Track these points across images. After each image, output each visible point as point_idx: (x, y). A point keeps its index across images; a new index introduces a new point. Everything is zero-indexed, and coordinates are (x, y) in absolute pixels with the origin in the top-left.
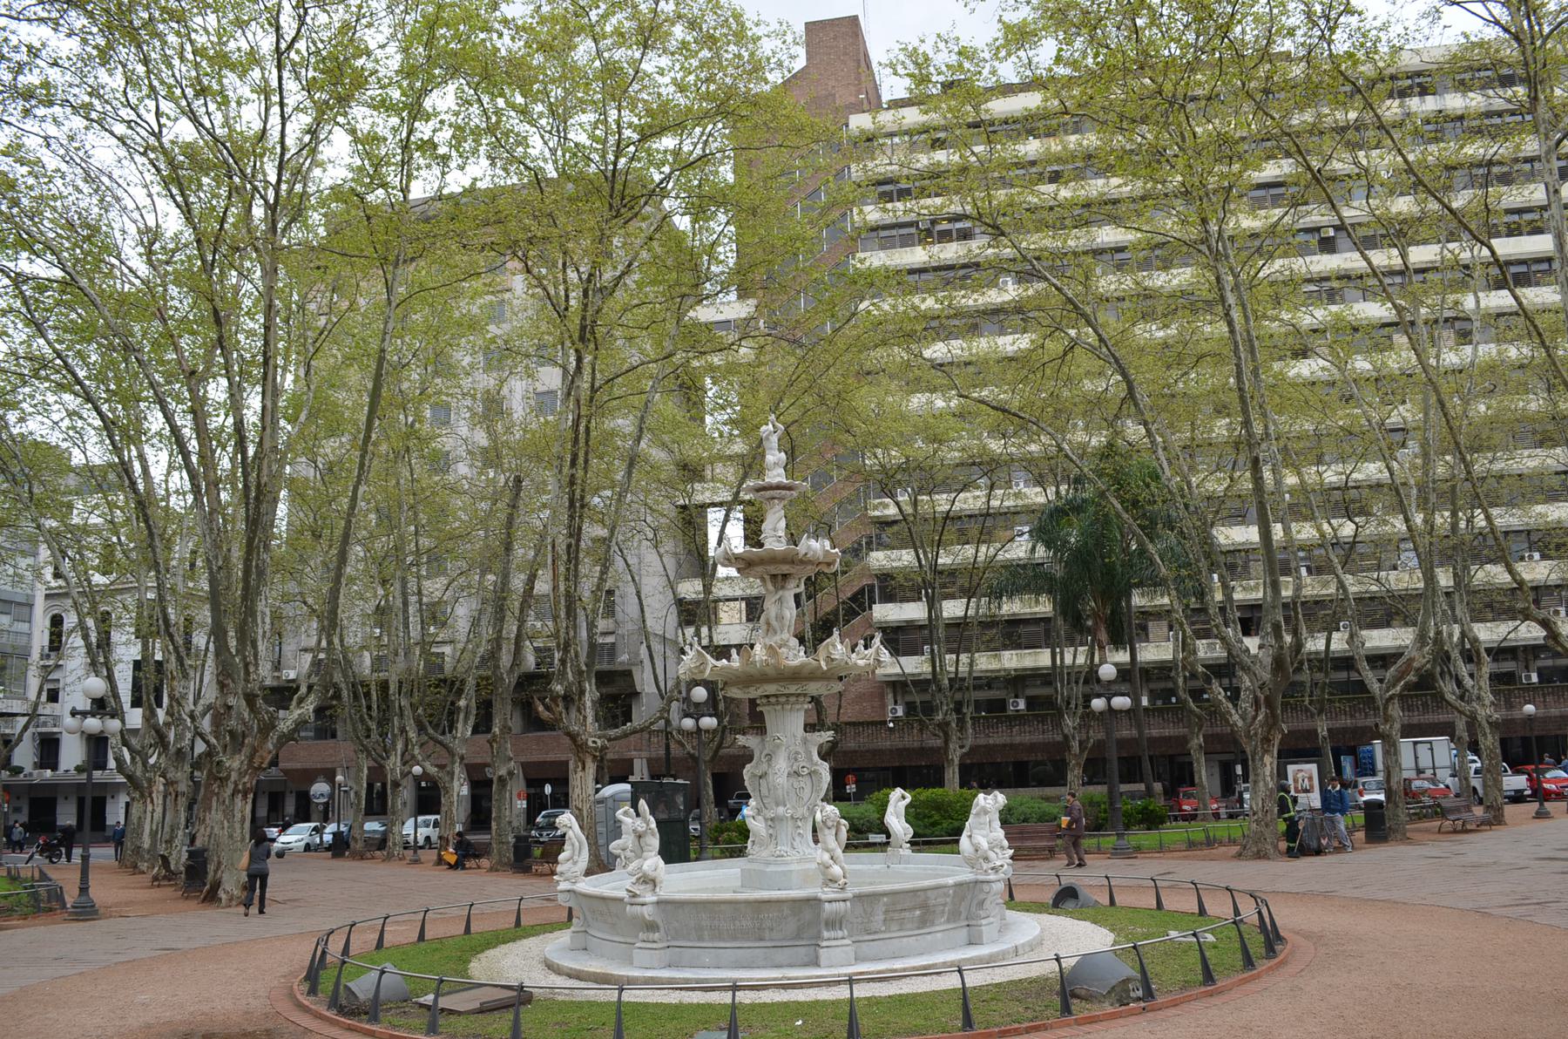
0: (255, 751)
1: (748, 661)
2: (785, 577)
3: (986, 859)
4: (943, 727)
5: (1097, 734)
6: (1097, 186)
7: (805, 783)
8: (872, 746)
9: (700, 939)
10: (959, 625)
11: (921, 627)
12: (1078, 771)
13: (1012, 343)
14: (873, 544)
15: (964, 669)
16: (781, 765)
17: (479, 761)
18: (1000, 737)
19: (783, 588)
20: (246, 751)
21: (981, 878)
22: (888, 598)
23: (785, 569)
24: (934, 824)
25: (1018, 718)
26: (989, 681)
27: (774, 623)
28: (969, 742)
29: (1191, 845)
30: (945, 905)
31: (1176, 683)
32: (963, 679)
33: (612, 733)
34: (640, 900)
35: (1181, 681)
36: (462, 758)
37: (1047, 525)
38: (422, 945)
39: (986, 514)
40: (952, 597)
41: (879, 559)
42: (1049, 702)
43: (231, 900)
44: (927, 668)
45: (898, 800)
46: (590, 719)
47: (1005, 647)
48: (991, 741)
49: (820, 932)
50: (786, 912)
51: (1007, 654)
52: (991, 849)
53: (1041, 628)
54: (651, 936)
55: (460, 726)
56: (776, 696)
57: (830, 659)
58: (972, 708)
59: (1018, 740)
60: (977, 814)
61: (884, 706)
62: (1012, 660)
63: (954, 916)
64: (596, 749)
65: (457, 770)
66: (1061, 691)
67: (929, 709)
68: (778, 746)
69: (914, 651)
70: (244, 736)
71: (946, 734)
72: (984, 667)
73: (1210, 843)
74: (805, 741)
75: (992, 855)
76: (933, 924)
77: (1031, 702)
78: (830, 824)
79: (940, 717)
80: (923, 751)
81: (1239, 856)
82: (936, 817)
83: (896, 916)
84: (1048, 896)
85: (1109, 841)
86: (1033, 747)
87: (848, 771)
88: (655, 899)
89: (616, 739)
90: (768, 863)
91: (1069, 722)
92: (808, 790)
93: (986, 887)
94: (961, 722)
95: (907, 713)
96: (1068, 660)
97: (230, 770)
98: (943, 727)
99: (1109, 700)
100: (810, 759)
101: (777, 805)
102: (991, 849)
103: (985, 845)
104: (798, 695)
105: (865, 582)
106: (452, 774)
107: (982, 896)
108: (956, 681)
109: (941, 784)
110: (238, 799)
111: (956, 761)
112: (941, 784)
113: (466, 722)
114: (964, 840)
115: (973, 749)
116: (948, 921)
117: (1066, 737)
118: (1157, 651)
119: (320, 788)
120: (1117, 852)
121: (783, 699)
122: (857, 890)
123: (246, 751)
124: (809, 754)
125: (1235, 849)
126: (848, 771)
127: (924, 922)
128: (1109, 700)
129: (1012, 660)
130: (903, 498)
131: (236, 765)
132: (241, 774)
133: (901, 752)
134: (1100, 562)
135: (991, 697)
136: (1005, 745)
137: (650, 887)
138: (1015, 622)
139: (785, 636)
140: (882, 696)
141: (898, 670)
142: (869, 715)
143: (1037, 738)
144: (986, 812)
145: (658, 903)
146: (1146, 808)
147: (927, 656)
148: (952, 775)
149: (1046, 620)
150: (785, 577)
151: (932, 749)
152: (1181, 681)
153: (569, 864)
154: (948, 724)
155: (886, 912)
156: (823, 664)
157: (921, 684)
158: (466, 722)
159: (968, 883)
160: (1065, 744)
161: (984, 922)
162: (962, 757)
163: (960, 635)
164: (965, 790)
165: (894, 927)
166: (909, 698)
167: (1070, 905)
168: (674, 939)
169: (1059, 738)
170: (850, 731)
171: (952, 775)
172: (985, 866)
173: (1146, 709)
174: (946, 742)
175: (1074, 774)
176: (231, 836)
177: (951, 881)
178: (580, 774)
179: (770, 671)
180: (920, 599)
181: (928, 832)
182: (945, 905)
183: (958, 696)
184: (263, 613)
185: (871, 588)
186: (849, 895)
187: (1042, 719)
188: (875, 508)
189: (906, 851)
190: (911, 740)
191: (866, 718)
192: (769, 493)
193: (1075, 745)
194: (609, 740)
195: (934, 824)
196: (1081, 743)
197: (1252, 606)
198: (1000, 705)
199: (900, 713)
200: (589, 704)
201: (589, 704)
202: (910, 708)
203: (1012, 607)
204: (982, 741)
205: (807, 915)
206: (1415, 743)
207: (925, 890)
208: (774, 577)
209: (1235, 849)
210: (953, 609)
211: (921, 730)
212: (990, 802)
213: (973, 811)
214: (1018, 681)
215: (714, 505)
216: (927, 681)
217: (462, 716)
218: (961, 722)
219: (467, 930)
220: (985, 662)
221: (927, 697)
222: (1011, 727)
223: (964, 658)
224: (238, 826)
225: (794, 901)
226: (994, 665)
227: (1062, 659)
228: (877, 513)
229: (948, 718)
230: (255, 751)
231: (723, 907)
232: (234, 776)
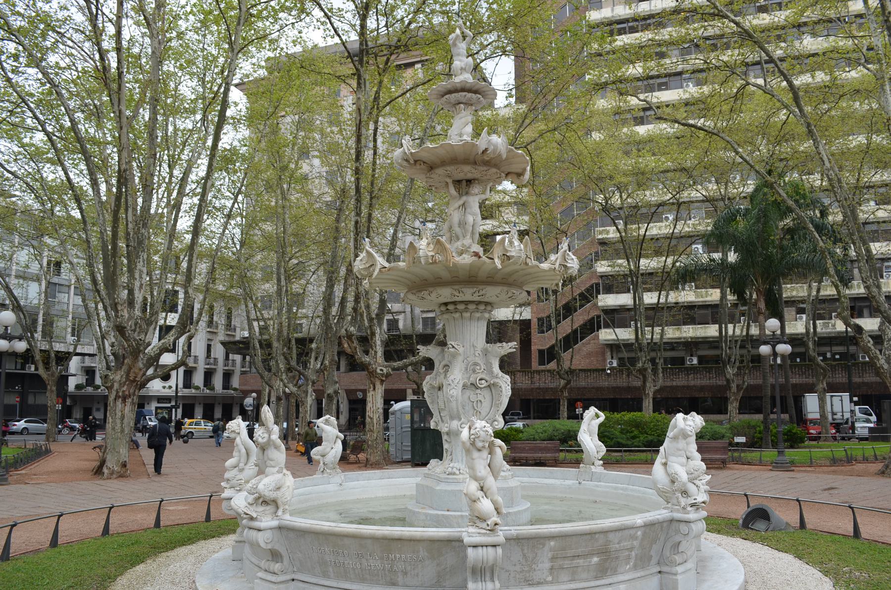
0: (130, 369)
1: (416, 261)
2: (469, 182)
3: (685, 493)
4: (642, 371)
5: (750, 380)
6: (687, 295)
7: (485, 397)
8: (596, 385)
9: (325, 575)
10: (655, 309)
11: (629, 310)
12: (736, 404)
13: (692, 90)
14: (598, 257)
15: (657, 337)
16: (457, 376)
17: (354, 388)
18: (680, 381)
19: (467, 193)
20: (125, 368)
21: (678, 515)
22: (609, 290)
23: (467, 172)
24: (634, 438)
25: (693, 368)
26: (672, 345)
27: (457, 229)
28: (660, 383)
29: (834, 461)
30: (631, 549)
31: (807, 348)
32: (655, 344)
33: (396, 364)
34: (256, 524)
35: (811, 345)
36: (313, 383)
37: (716, 239)
38: (107, 539)
39: (670, 237)
40: (649, 290)
41: (602, 267)
42: (717, 359)
43: (112, 473)
44: (633, 337)
45: (591, 421)
46: (380, 353)
47: (685, 324)
48: (674, 384)
49: (466, 580)
50: (423, 553)
51: (685, 328)
52: (691, 481)
53: (709, 312)
54: (277, 567)
55: (312, 360)
56: (455, 303)
57: (506, 257)
58: (662, 361)
59: (692, 383)
60: (675, 438)
61: (605, 360)
62: (690, 332)
63: (642, 561)
64: (382, 375)
65: (310, 390)
66: (725, 352)
67: (633, 361)
68: (454, 356)
69: (624, 325)
70: (124, 357)
71: (644, 377)
72: (671, 336)
73: (850, 460)
74: (486, 353)
75: (692, 488)
76: (615, 572)
77: (701, 359)
78: (479, 444)
79: (640, 365)
80: (629, 389)
81: (882, 473)
82: (636, 433)
83: (567, 563)
84: (740, 511)
85: (770, 454)
86: (702, 388)
87: (577, 400)
88: (275, 523)
89: (397, 369)
90: (440, 481)
91: (730, 371)
92: (486, 403)
93: (683, 528)
94: (655, 371)
95: (619, 365)
96: (730, 332)
97: (113, 381)
98: (642, 371)
99: (774, 347)
100: (491, 372)
101: (452, 418)
102: (691, 481)
103: (684, 476)
104: (479, 303)
105: (594, 281)
106: (306, 392)
107: (678, 538)
108: (653, 346)
109: (640, 410)
110: (119, 402)
111: (651, 395)
112: (640, 410)
113: (316, 359)
114: (658, 467)
115: (662, 389)
116: (635, 567)
117: (728, 381)
118: (798, 326)
119: (249, 401)
120: (777, 466)
121: (461, 307)
122: (514, 531)
123: (125, 368)
124: (489, 365)
125: (879, 466)
126: (577, 400)
127: (603, 571)
128: (774, 347)
129: (690, 332)
130: (621, 226)
131: (118, 378)
132: (121, 385)
133: (615, 389)
134: (765, 248)
135: (675, 355)
136: (684, 387)
137: (270, 509)
138: (691, 307)
139: (467, 241)
140: (603, 354)
141: (614, 337)
142: (595, 365)
143: (705, 382)
144: (685, 436)
145: (280, 528)
146: (790, 431)
147: (633, 328)
148: (648, 404)
149: (716, 306)
150: (469, 182)
151: (635, 388)
152: (811, 345)
153: (235, 472)
154: (646, 370)
155: (553, 559)
156: (498, 263)
157: (628, 346)
158: (316, 359)
159: (660, 523)
160: (728, 387)
161: (680, 569)
162: (655, 393)
163: (655, 315)
164: (656, 414)
165: (564, 576)
166: (621, 355)
167: (760, 525)
168: (300, 571)
169: (721, 382)
170: (582, 375)
171: (648, 404)
172: (683, 501)
173: (779, 365)
174: (644, 382)
175: (733, 406)
176: (113, 429)
177: (639, 519)
178: (372, 393)
179: (445, 274)
180: (629, 291)
181: (629, 443)
182: (631, 549)
183: (653, 354)
184: (141, 271)
185: (597, 284)
186: (500, 538)
187: (709, 370)
188: (601, 233)
189: (598, 468)
190: (622, 381)
191: (593, 367)
192: (454, 97)
193: (734, 387)
194: (394, 369)
195: (634, 438)
196: (738, 386)
197: (855, 298)
198: (682, 361)
199: (615, 364)
200: (378, 343)
201: (378, 343)
202: (621, 361)
203: (687, 295)
204: (669, 384)
205: (450, 559)
206: (832, 396)
207: (605, 532)
208: (458, 183)
209: (879, 466)
210: (650, 298)
211: (628, 376)
212: (688, 423)
213: (670, 434)
214: (692, 345)
215: (498, 234)
216: (632, 344)
217: (313, 355)
218: (655, 371)
219: (208, 518)
220: (672, 333)
221: (632, 355)
222: (688, 375)
223: (657, 330)
224: (118, 421)
225: (432, 541)
226: (677, 334)
227: (726, 332)
228: (600, 237)
229: (646, 365)
230: (130, 369)
231: (347, 541)
232: (116, 386)
